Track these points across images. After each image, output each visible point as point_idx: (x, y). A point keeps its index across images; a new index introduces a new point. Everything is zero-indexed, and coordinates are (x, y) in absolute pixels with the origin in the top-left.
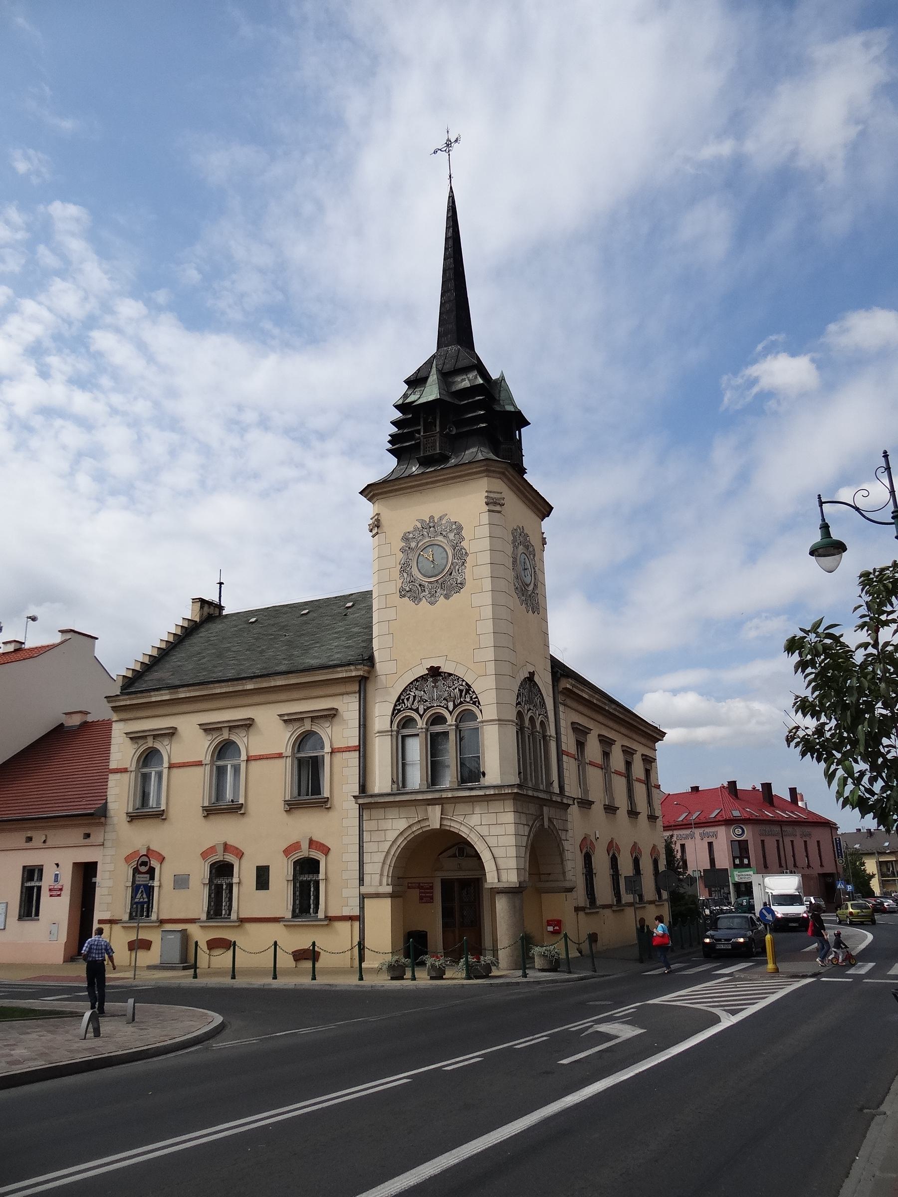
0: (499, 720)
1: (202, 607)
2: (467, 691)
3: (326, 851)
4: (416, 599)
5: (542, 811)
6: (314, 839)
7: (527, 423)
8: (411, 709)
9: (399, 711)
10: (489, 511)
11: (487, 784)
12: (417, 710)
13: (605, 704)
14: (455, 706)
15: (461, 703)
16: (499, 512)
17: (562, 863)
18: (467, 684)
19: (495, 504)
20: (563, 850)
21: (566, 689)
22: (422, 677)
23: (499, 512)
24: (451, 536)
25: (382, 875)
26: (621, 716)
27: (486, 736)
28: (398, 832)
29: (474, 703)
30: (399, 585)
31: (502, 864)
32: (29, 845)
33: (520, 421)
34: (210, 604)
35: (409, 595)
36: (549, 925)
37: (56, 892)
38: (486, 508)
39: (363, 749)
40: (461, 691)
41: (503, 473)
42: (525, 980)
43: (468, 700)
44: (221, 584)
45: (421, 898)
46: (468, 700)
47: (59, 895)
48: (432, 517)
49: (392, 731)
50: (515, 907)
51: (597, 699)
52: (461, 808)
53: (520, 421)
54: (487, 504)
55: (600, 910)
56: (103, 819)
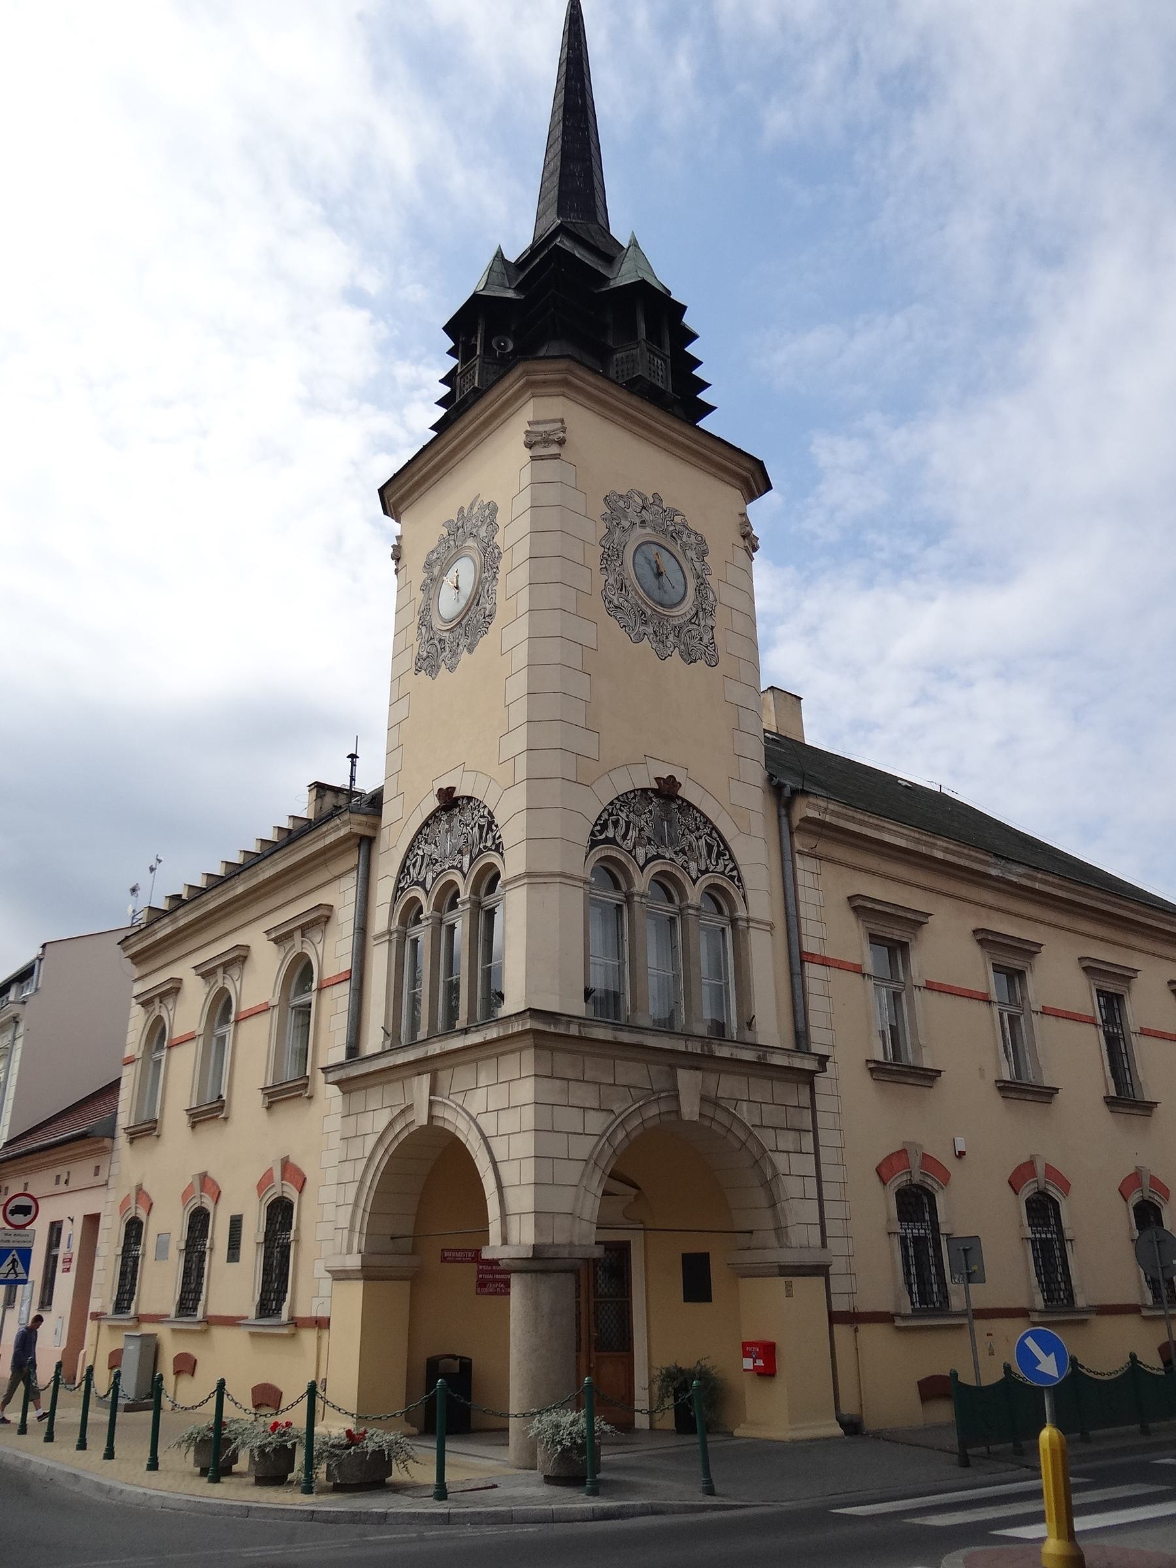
0: (528, 875)
1: (319, 797)
2: (490, 829)
4: (433, 669)
5: (675, 1077)
6: (292, 1160)
7: (684, 308)
9: (403, 889)
10: (533, 458)
11: (503, 1015)
12: (422, 884)
13: (987, 863)
15: (481, 852)
16: (556, 457)
17: (773, 1205)
19: (546, 442)
20: (776, 1175)
21: (807, 820)
22: (433, 816)
23: (556, 457)
25: (351, 1230)
26: (1060, 893)
27: (379, 891)
28: (375, 1138)
30: (416, 652)
31: (513, 1206)
32: (62, 1187)
33: (682, 309)
34: (337, 791)
35: (426, 664)
36: (746, 1355)
38: (528, 453)
39: (358, 977)
40: (481, 827)
41: (566, 383)
42: (440, 1508)
43: (489, 844)
44: (353, 757)
45: (482, 1284)
46: (489, 844)
49: (390, 932)
50: (537, 1307)
51: (946, 850)
52: (462, 1077)
53: (682, 309)
54: (529, 445)
55: (1092, 1317)
56: (107, 1142)
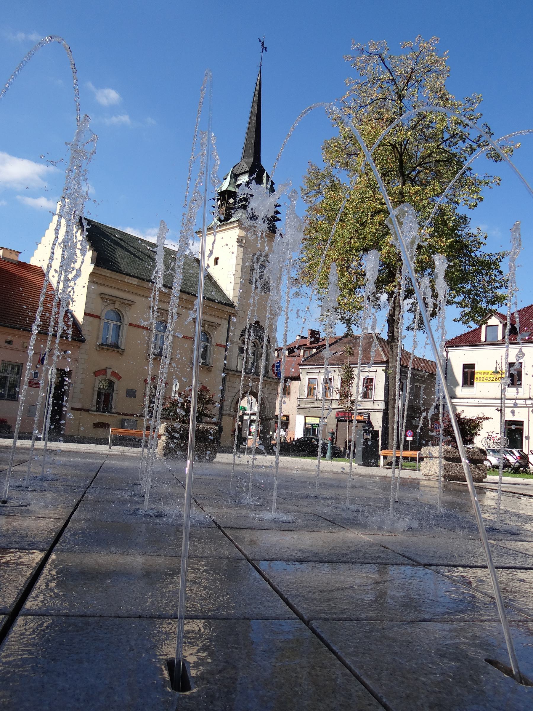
3: (119, 378)
38: (237, 244)
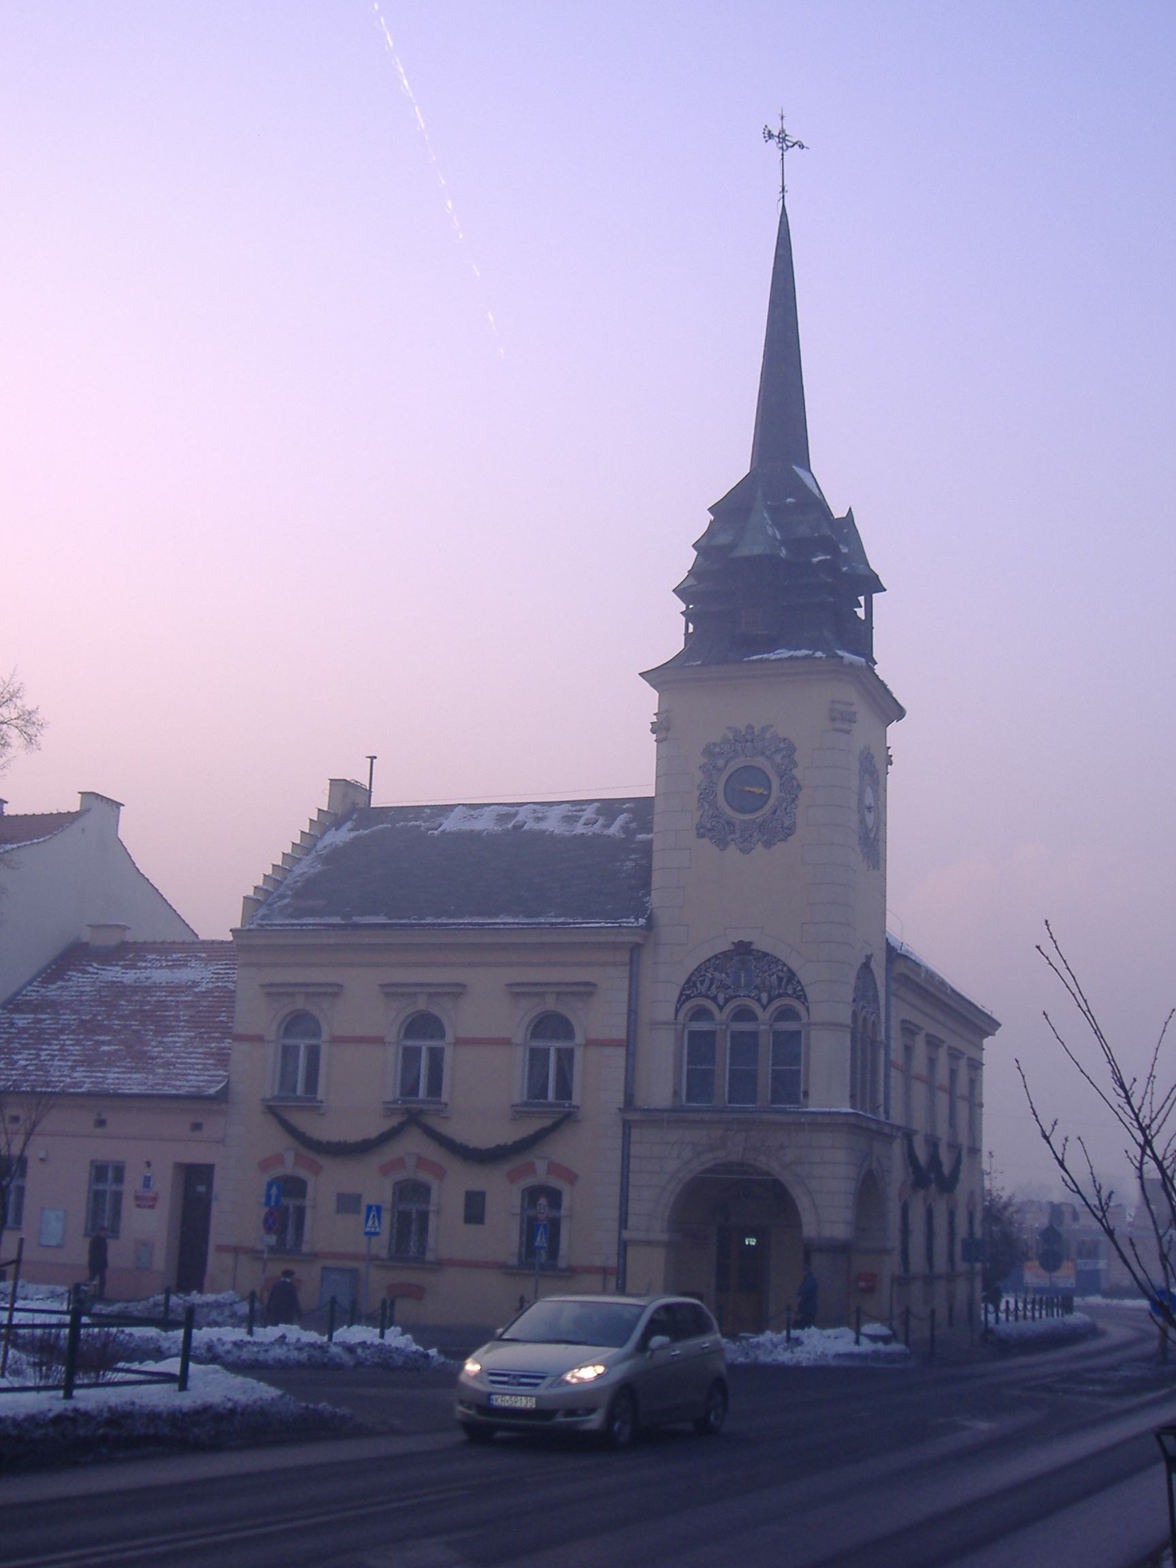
3: (572, 1178)
4: (722, 844)
8: (707, 997)
12: (714, 999)
14: (771, 1000)
18: (790, 970)
24: (778, 758)
29: (798, 998)
37: (146, 1201)
47: (152, 1207)
48: (750, 727)
